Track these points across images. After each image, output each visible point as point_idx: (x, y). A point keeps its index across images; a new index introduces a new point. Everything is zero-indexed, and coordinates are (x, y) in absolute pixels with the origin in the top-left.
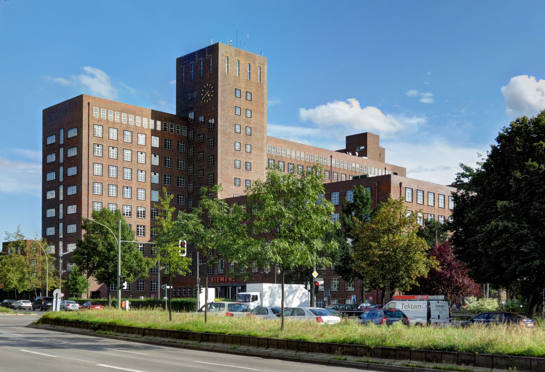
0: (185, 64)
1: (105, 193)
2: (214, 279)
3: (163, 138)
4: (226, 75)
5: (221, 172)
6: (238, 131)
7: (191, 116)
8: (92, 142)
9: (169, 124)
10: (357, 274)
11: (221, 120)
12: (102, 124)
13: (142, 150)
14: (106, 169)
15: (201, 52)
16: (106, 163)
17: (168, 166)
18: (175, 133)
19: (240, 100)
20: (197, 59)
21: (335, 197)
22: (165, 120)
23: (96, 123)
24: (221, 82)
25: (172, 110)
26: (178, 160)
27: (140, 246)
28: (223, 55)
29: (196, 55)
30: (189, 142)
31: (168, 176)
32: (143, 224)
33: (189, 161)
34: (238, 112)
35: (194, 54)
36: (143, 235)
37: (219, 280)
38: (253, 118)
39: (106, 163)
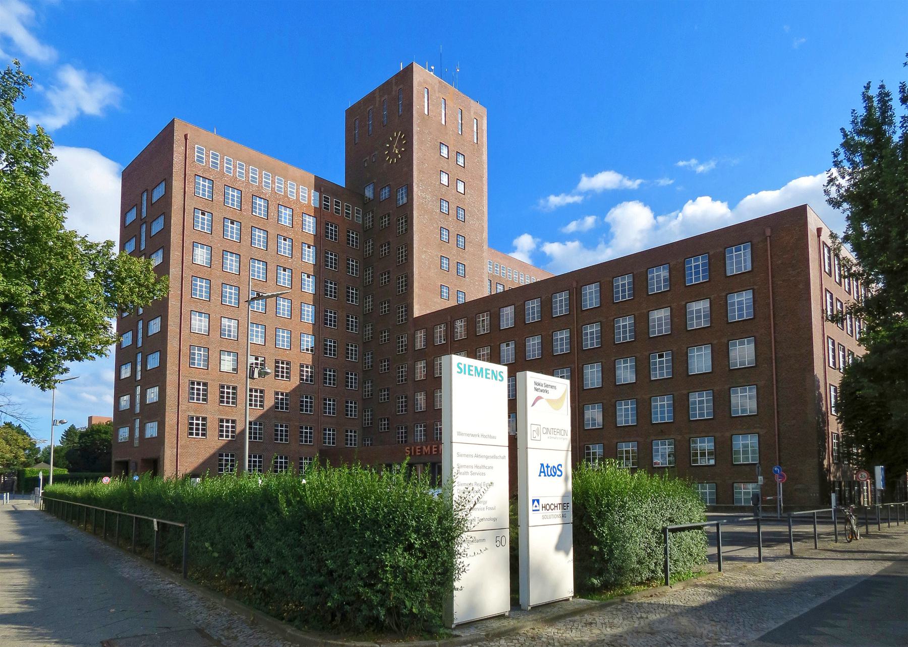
0: (356, 116)
1: (215, 297)
2: (410, 450)
3: (322, 309)
4: (426, 117)
5: (419, 273)
6: (445, 210)
7: (369, 193)
8: (190, 205)
9: (332, 201)
10: (659, 632)
11: (418, 186)
12: (211, 178)
13: (285, 235)
14: (218, 255)
15: (386, 87)
16: (218, 247)
17: (330, 384)
18: (342, 216)
19: (448, 163)
20: (378, 99)
21: (591, 293)
22: (326, 192)
23: (200, 173)
24: (418, 126)
25: (339, 179)
26: (347, 402)
27: (280, 397)
28: (420, 84)
29: (377, 95)
30: (366, 233)
31: (330, 400)
32: (286, 359)
33: (366, 262)
34: (445, 237)
35: (373, 93)
36: (287, 377)
37: (421, 452)
38: (468, 196)
39: (218, 247)
